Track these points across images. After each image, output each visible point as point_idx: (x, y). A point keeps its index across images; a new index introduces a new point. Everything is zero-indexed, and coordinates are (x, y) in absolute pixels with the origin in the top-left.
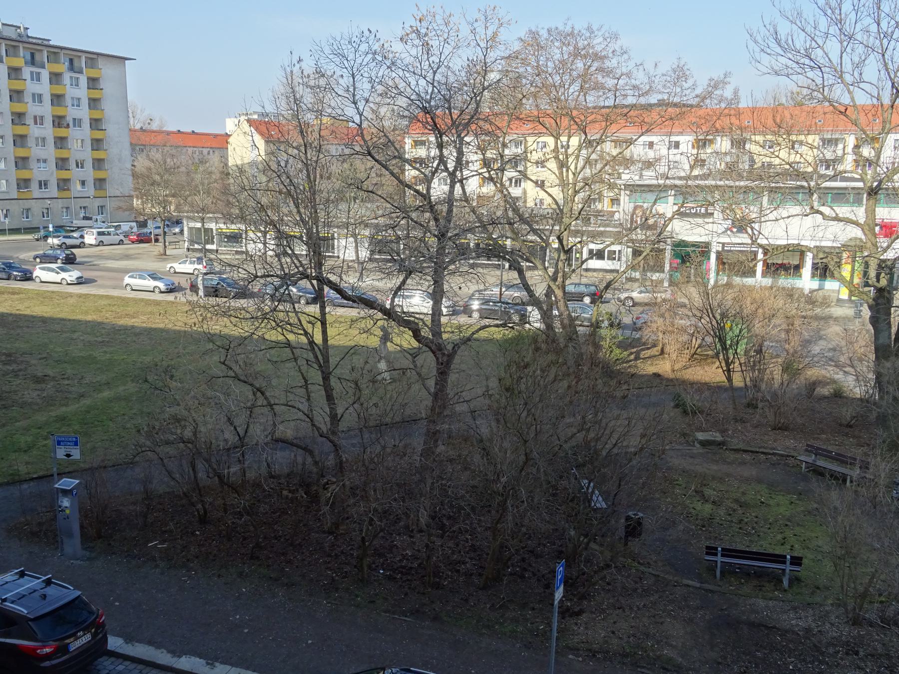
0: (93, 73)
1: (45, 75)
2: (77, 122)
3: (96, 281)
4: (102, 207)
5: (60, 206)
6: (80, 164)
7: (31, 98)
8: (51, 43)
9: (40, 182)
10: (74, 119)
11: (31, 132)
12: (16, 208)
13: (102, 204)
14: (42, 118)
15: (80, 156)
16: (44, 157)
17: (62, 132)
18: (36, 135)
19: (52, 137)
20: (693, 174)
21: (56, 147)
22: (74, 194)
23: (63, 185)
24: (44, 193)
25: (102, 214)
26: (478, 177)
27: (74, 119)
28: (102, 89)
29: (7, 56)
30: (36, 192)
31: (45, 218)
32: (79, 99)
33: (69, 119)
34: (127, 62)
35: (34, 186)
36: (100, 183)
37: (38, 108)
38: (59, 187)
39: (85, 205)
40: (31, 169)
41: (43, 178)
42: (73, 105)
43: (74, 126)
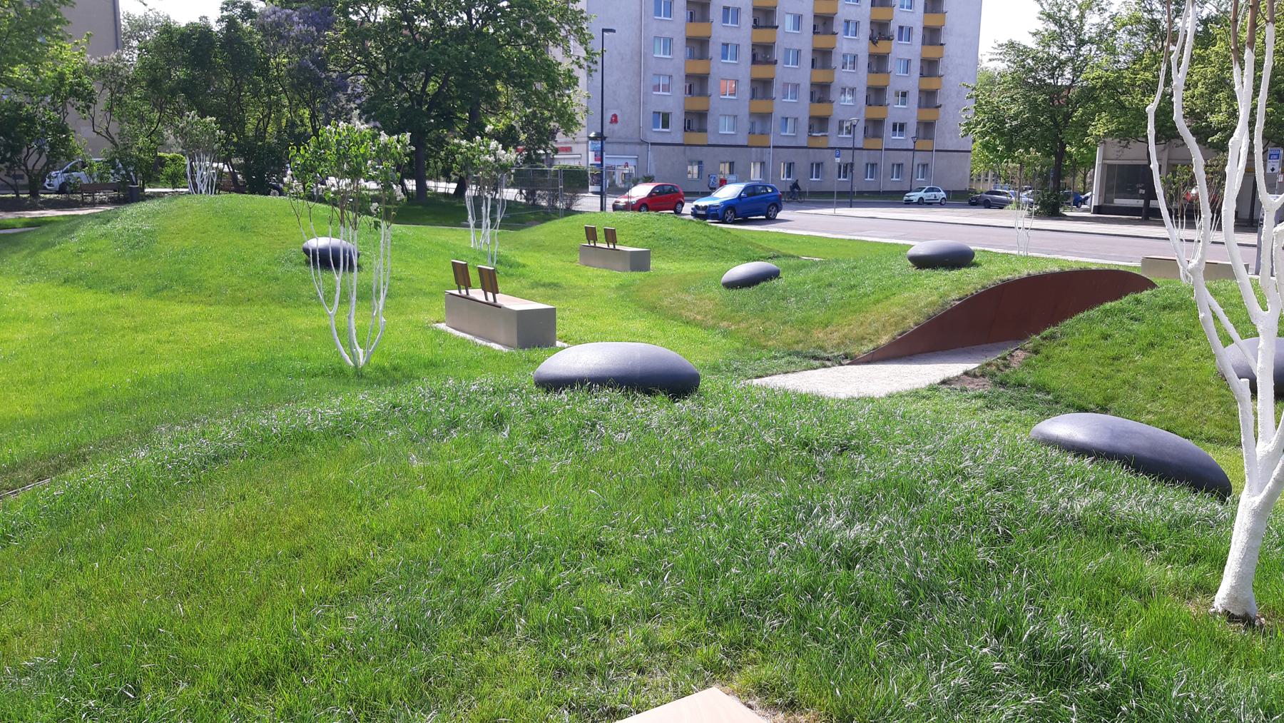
2: (905, 32)
3: (1148, 284)
4: (873, 165)
5: (865, 161)
9: (895, 126)
11: (838, 45)
12: (802, 161)
13: (924, 162)
14: (910, 29)
15: (902, 87)
16: (851, 86)
18: (845, 51)
20: (287, 104)
23: (875, 126)
27: (901, 28)
30: (891, 138)
31: (842, 179)
35: (888, 128)
36: (927, 127)
37: (852, 10)
38: (688, 128)
39: (900, 162)
40: (831, 102)
41: (898, 121)
43: (900, 39)
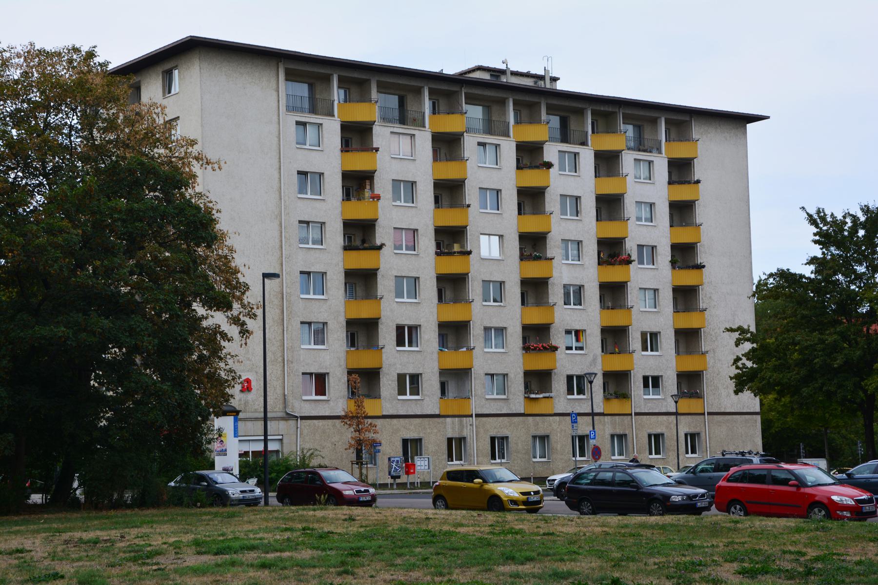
0: (681, 151)
1: (587, 157)
6: (651, 340)
7: (558, 206)
8: (560, 86)
10: (640, 247)
11: (555, 274)
17: (614, 274)
19: (433, 276)
21: (603, 305)
22: (476, 406)
24: (408, 403)
25: (693, 452)
26: (295, 450)
28: (698, 182)
29: (593, 132)
32: (651, 205)
33: (631, 246)
34: (750, 126)
37: (572, 226)
42: (639, 219)
